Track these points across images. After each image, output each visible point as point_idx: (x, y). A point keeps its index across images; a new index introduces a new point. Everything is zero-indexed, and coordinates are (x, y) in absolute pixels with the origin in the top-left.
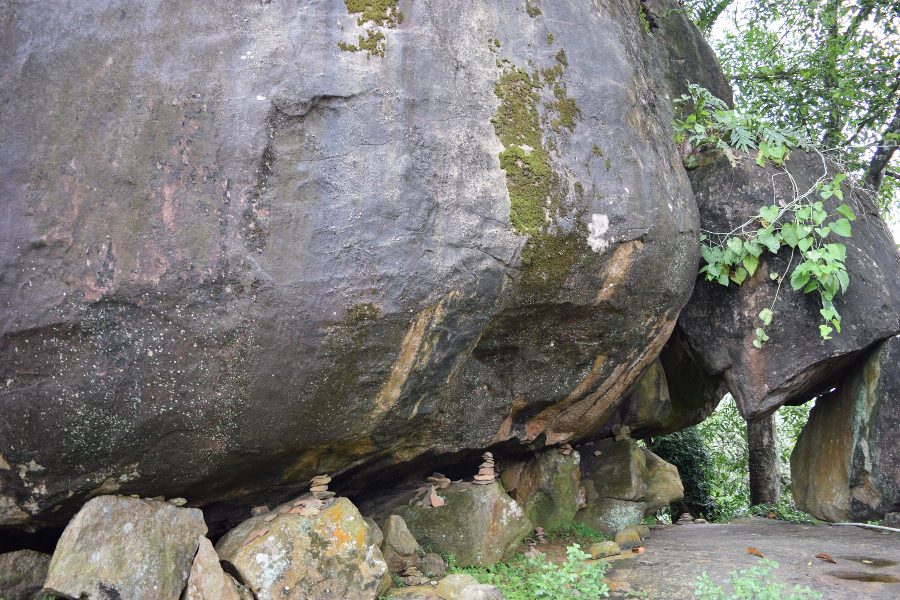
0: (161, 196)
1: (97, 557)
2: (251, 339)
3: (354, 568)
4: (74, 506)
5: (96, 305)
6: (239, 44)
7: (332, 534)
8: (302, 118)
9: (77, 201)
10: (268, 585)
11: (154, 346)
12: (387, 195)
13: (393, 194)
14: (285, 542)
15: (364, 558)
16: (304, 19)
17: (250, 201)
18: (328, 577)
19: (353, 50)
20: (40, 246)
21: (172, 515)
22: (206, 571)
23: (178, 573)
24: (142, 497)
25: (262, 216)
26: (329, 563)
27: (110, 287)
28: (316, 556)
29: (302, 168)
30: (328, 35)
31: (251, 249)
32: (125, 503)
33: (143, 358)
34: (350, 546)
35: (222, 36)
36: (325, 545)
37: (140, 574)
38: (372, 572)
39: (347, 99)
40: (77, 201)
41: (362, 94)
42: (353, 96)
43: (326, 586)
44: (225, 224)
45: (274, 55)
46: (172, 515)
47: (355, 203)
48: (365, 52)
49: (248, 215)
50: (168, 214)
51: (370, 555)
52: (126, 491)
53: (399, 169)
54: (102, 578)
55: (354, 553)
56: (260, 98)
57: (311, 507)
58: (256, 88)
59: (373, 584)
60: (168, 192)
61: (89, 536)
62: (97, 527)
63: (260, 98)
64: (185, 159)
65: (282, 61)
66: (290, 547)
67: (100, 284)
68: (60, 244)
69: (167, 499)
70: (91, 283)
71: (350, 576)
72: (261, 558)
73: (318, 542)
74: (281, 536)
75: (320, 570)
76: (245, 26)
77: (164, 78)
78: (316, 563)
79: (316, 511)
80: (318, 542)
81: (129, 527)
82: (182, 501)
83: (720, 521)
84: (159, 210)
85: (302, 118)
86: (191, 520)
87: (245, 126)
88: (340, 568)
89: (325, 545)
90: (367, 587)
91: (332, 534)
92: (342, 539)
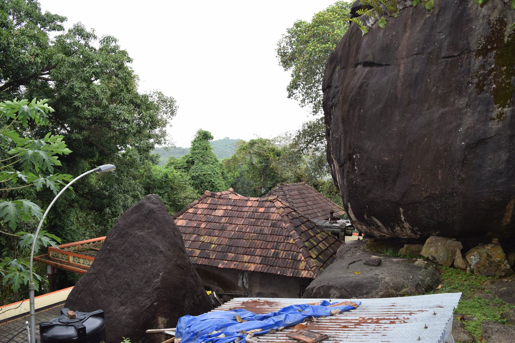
0: (438, 172)
1: (431, 249)
2: (461, 206)
3: (500, 265)
4: (427, 237)
5: (425, 198)
6: (458, 126)
7: (493, 255)
8: (475, 147)
9: (420, 175)
10: (473, 264)
11: (438, 207)
12: (500, 167)
13: (502, 167)
14: (479, 254)
15: (503, 263)
16: (479, 111)
17: (460, 172)
18: (491, 266)
19: (494, 119)
20: (413, 185)
21: (452, 242)
22: (458, 257)
23: (452, 257)
24: (443, 237)
25: (463, 176)
26: (492, 262)
27: (428, 194)
28: (488, 260)
29: (474, 162)
30: (487, 115)
31: (460, 184)
32: (439, 238)
33: (436, 209)
34: (498, 259)
35: (454, 124)
36: (491, 257)
37: (441, 255)
38: (505, 267)
39: (489, 138)
40: (420, 175)
41: (495, 135)
42: (492, 137)
43: (490, 268)
44: (454, 178)
45: (468, 129)
46: (452, 242)
47: (489, 171)
48: (498, 120)
49: (459, 176)
50: (440, 177)
51: (505, 263)
52: (439, 235)
53: (505, 159)
54: (432, 254)
55: (499, 261)
56: (463, 143)
57: (489, 247)
58: (463, 140)
59: (504, 271)
60: (440, 171)
61: (430, 244)
62: (431, 243)
63: (463, 143)
64: (444, 163)
65: (470, 131)
66: (480, 256)
67: (426, 193)
68: (417, 184)
69: (451, 238)
70: (424, 193)
71: (498, 267)
72: (472, 257)
73: (489, 256)
74: (479, 253)
75: (489, 264)
76: (461, 119)
77: (439, 141)
78: (488, 261)
79: (490, 248)
80: (489, 256)
81: (440, 244)
82: (454, 239)
83: (41, 227)
84: (438, 176)
85: (475, 147)
86: (457, 245)
87: (459, 152)
88: (495, 264)
89: (491, 257)
90: (502, 271)
91: (493, 255)
92: (496, 257)
